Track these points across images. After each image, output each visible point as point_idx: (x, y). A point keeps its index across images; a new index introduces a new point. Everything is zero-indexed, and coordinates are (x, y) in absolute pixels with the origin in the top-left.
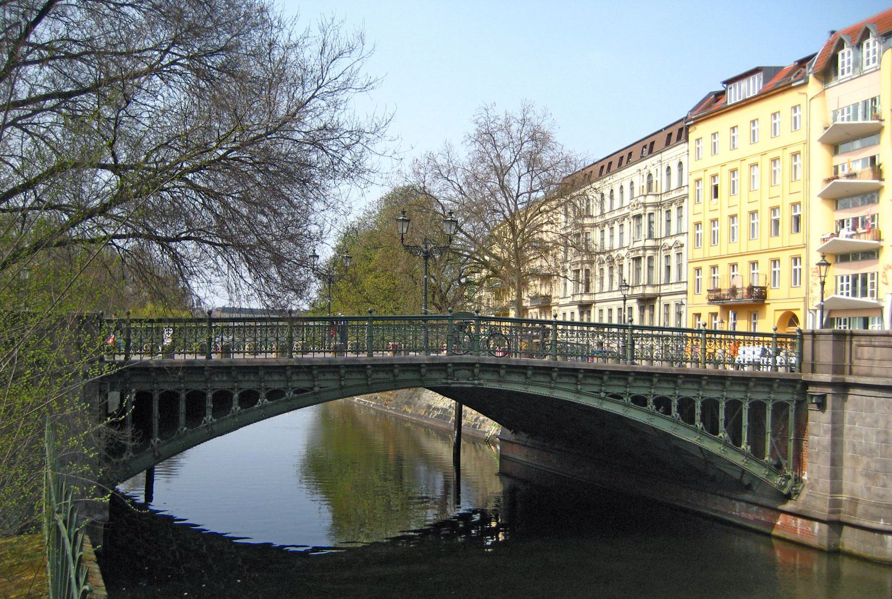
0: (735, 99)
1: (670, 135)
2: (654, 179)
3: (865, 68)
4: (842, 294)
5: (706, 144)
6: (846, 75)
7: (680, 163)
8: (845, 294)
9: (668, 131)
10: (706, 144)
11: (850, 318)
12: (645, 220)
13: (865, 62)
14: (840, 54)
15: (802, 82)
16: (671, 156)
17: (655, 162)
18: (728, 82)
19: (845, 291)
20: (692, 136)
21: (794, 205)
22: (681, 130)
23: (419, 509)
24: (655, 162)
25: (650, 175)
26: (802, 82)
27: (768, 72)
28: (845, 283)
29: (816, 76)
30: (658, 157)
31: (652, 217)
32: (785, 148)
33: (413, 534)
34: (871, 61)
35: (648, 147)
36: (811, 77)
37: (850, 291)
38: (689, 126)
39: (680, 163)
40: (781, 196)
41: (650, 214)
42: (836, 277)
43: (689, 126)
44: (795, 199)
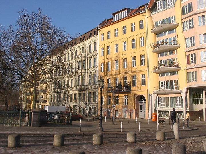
0: (124, 12)
1: (91, 34)
2: (85, 49)
3: (168, 7)
4: (165, 88)
5: (105, 36)
6: (160, 9)
7: (95, 43)
8: (163, 88)
9: (90, 32)
10: (105, 36)
11: (166, 97)
12: (81, 63)
13: (167, 5)
14: (157, 2)
15: (144, 11)
16: (91, 40)
17: (85, 43)
18: (113, 14)
19: (163, 87)
20: (100, 33)
21: (142, 56)
22: (95, 32)
23: (94, 101)
24: (85, 43)
25: (83, 48)
26: (144, 11)
27: (130, 11)
28: (163, 84)
29: (149, 10)
30: (87, 41)
31: (84, 61)
32: (137, 35)
33: (86, 98)
34: (170, 4)
35: (82, 38)
36: (147, 10)
37: (166, 87)
38: (98, 30)
39: (95, 43)
40: (136, 52)
41: (83, 61)
42: (160, 82)
43: (98, 30)
44: (142, 53)
